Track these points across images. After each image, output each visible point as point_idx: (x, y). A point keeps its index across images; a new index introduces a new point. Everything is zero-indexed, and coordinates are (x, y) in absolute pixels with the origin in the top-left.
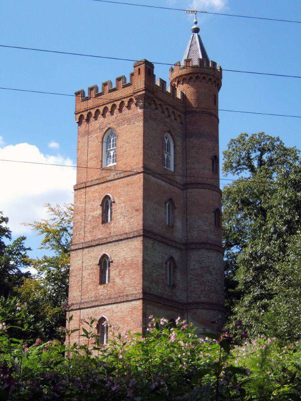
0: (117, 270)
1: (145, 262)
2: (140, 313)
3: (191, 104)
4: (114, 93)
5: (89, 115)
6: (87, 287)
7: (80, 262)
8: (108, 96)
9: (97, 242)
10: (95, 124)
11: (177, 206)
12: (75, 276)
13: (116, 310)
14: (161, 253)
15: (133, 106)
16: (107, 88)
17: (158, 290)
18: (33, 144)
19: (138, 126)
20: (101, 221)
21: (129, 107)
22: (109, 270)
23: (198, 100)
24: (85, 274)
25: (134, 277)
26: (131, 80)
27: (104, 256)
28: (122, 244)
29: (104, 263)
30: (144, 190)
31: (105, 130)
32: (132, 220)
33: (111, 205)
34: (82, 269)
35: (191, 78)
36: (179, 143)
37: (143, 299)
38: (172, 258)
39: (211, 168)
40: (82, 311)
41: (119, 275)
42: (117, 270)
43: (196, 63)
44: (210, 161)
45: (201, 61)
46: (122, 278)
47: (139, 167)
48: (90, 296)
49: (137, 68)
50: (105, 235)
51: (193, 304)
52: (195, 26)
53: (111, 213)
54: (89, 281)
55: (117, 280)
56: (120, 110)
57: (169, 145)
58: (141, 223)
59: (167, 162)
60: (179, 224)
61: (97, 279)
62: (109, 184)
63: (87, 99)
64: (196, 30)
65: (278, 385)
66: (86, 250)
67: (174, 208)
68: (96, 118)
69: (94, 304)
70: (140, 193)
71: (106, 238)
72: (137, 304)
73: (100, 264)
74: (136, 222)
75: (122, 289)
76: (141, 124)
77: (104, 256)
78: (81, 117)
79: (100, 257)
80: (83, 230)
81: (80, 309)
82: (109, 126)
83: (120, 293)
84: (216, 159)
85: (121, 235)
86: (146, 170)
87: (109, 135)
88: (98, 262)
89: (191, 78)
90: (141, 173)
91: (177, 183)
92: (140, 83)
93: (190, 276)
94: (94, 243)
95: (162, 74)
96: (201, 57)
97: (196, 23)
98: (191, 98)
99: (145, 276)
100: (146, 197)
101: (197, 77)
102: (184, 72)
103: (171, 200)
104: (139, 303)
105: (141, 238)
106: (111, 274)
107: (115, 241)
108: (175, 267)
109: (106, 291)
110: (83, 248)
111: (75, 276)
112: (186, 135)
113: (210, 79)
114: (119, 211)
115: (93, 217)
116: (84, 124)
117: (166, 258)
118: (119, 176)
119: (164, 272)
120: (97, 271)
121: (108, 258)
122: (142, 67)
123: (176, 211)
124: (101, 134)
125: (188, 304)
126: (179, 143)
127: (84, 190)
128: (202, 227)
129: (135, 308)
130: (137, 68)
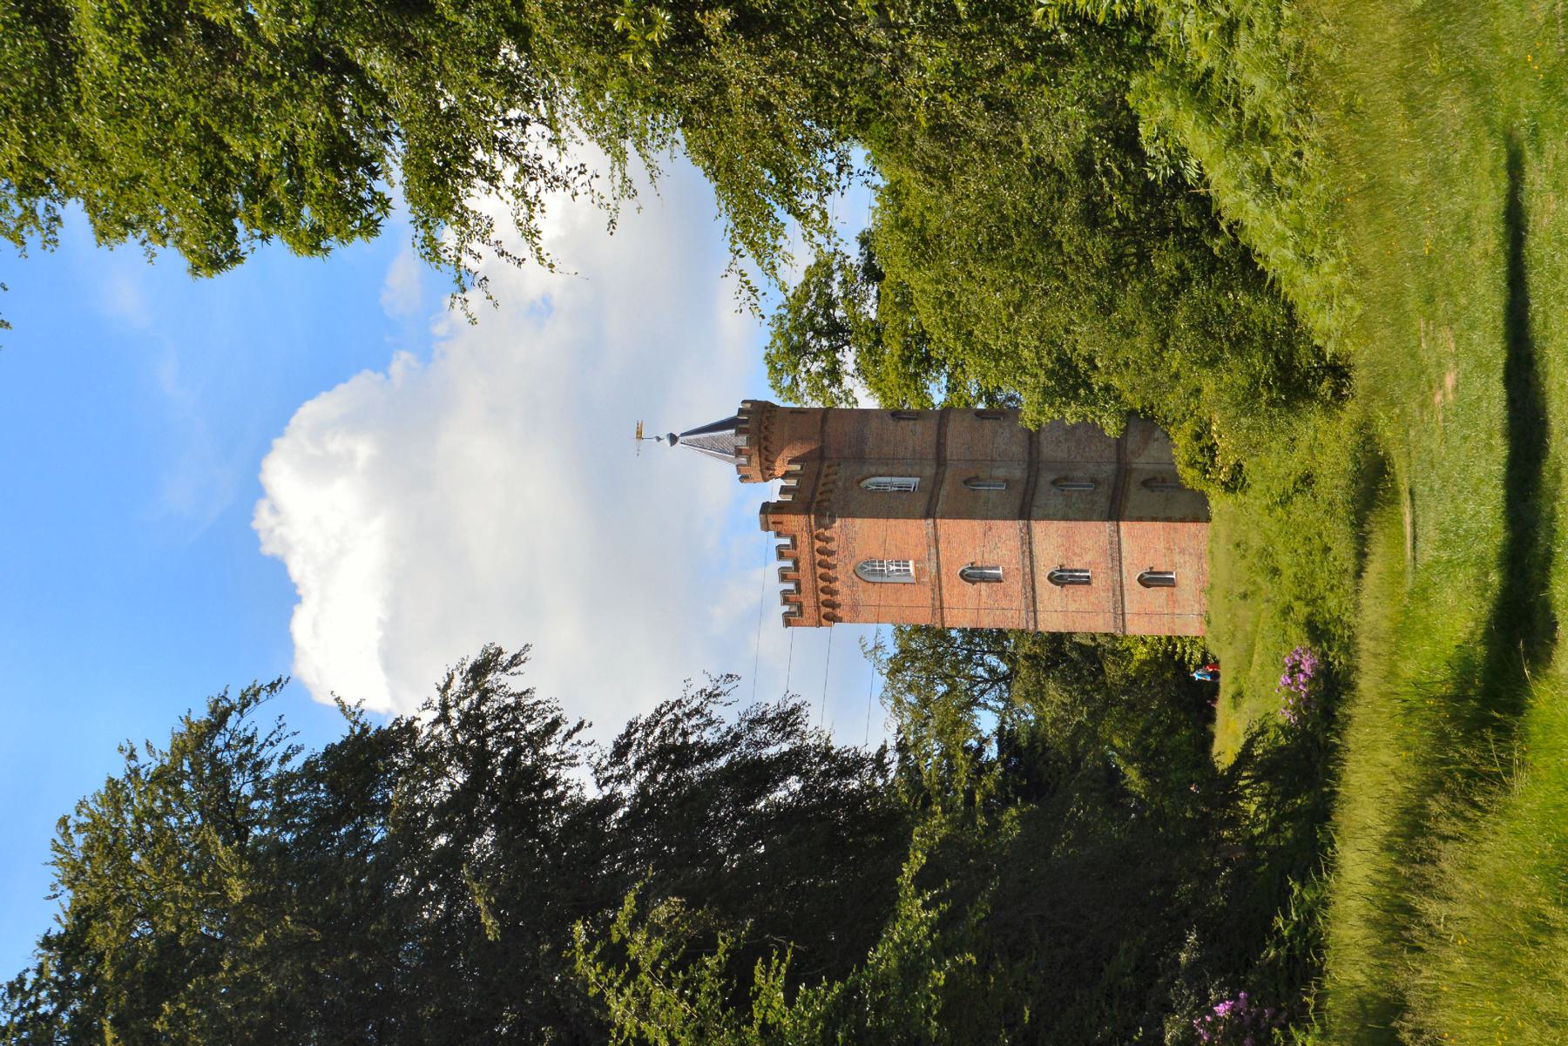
1: (1065, 518)
2: (1137, 525)
3: (811, 452)
5: (826, 604)
6: (1093, 604)
7: (1054, 615)
8: (806, 576)
9: (1029, 589)
10: (843, 597)
11: (973, 475)
12: (1074, 622)
14: (1047, 495)
15: (828, 533)
16: (791, 574)
17: (1103, 503)
18: (1547, 606)
19: (862, 526)
21: (828, 540)
22: (1076, 571)
23: (803, 439)
24: (1073, 607)
26: (786, 536)
27: (1051, 578)
28: (1036, 550)
29: (1061, 578)
30: (877, 517)
31: (856, 579)
32: (1003, 536)
33: (978, 568)
34: (1065, 612)
35: (766, 448)
36: (873, 470)
37: (1118, 520)
38: (1054, 483)
39: (911, 422)
41: (1080, 555)
43: (742, 441)
44: (902, 423)
45: (739, 432)
47: (1108, 526)
48: (1019, 602)
49: (771, 526)
50: (1019, 578)
51: (1118, 454)
52: (667, 442)
53: (1076, 571)
54: (1084, 601)
55: (1088, 558)
56: (831, 553)
57: (878, 485)
58: (1009, 523)
59: (904, 490)
60: (1001, 472)
61: (1083, 588)
62: (943, 571)
63: (800, 608)
64: (673, 439)
66: (1039, 606)
67: (977, 478)
68: (833, 593)
69: (1118, 593)
70: (964, 525)
71: (1024, 575)
73: (1063, 585)
74: (1009, 531)
76: (858, 521)
77: (1051, 578)
78: (826, 617)
79: (1051, 585)
80: (1006, 612)
81: (1123, 614)
82: (851, 572)
84: (793, 411)
85: (1023, 553)
86: (929, 514)
87: (868, 572)
88: (1059, 588)
89: (766, 448)
91: (937, 474)
92: (796, 522)
93: (1078, 459)
94: (1030, 595)
95: (772, 491)
96: (733, 431)
97: (659, 439)
98: (797, 451)
99: (1086, 518)
100: (970, 515)
101: (766, 439)
102: (755, 460)
103: (966, 482)
104: (1124, 526)
105: (1032, 522)
106: (1079, 568)
108: (1066, 478)
110: (1035, 612)
111: (1074, 622)
112: (860, 458)
113: (767, 418)
115: (989, 596)
116: (839, 612)
117: (1054, 490)
118: (934, 557)
119: (1076, 495)
120: (1071, 589)
121: (1052, 573)
122: (771, 518)
123: (981, 475)
124: (861, 584)
125: (1119, 461)
126: (873, 470)
127: (946, 612)
128: (919, 436)
129: (1130, 533)
130: (771, 526)
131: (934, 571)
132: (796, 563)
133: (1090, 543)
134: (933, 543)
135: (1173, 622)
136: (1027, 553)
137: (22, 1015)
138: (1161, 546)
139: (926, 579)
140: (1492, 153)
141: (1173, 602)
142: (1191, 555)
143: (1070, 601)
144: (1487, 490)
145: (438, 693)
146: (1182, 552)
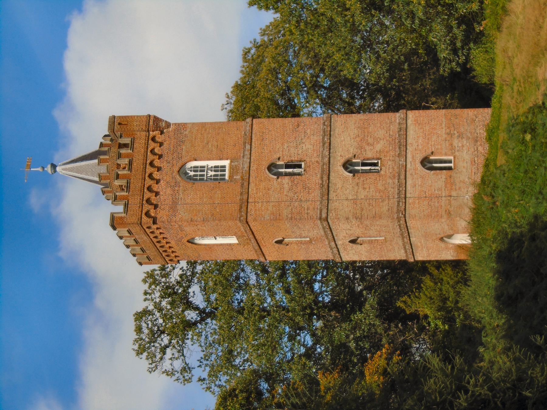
0: (367, 148)
4: (135, 165)
7: (346, 203)
13: (415, 146)
20: (152, 222)
24: (362, 194)
25: (379, 125)
28: (335, 141)
32: (308, 131)
40: (408, 195)
41: (372, 145)
42: (367, 148)
46: (377, 140)
53: (368, 159)
55: (378, 147)
65: (207, 351)
66: (332, 195)
69: (402, 177)
72: (413, 117)
75: (391, 140)
83: (395, 142)
90: (252, 121)
107: (251, 136)
109: (390, 163)
114: (292, 150)
131: (246, 168)
132: (131, 163)
133: (381, 133)
134: (248, 140)
135: (450, 203)
136: (327, 145)
137: (359, 73)
138: (442, 132)
139: (238, 177)
140: (180, 172)
141: (450, 184)
142: (468, 138)
143: (361, 189)
144: (475, 112)
145: (158, 178)
146: (461, 136)
